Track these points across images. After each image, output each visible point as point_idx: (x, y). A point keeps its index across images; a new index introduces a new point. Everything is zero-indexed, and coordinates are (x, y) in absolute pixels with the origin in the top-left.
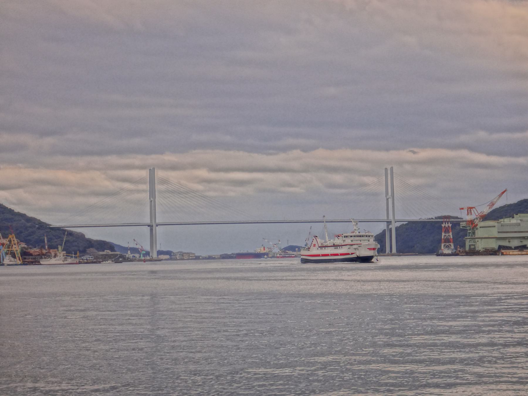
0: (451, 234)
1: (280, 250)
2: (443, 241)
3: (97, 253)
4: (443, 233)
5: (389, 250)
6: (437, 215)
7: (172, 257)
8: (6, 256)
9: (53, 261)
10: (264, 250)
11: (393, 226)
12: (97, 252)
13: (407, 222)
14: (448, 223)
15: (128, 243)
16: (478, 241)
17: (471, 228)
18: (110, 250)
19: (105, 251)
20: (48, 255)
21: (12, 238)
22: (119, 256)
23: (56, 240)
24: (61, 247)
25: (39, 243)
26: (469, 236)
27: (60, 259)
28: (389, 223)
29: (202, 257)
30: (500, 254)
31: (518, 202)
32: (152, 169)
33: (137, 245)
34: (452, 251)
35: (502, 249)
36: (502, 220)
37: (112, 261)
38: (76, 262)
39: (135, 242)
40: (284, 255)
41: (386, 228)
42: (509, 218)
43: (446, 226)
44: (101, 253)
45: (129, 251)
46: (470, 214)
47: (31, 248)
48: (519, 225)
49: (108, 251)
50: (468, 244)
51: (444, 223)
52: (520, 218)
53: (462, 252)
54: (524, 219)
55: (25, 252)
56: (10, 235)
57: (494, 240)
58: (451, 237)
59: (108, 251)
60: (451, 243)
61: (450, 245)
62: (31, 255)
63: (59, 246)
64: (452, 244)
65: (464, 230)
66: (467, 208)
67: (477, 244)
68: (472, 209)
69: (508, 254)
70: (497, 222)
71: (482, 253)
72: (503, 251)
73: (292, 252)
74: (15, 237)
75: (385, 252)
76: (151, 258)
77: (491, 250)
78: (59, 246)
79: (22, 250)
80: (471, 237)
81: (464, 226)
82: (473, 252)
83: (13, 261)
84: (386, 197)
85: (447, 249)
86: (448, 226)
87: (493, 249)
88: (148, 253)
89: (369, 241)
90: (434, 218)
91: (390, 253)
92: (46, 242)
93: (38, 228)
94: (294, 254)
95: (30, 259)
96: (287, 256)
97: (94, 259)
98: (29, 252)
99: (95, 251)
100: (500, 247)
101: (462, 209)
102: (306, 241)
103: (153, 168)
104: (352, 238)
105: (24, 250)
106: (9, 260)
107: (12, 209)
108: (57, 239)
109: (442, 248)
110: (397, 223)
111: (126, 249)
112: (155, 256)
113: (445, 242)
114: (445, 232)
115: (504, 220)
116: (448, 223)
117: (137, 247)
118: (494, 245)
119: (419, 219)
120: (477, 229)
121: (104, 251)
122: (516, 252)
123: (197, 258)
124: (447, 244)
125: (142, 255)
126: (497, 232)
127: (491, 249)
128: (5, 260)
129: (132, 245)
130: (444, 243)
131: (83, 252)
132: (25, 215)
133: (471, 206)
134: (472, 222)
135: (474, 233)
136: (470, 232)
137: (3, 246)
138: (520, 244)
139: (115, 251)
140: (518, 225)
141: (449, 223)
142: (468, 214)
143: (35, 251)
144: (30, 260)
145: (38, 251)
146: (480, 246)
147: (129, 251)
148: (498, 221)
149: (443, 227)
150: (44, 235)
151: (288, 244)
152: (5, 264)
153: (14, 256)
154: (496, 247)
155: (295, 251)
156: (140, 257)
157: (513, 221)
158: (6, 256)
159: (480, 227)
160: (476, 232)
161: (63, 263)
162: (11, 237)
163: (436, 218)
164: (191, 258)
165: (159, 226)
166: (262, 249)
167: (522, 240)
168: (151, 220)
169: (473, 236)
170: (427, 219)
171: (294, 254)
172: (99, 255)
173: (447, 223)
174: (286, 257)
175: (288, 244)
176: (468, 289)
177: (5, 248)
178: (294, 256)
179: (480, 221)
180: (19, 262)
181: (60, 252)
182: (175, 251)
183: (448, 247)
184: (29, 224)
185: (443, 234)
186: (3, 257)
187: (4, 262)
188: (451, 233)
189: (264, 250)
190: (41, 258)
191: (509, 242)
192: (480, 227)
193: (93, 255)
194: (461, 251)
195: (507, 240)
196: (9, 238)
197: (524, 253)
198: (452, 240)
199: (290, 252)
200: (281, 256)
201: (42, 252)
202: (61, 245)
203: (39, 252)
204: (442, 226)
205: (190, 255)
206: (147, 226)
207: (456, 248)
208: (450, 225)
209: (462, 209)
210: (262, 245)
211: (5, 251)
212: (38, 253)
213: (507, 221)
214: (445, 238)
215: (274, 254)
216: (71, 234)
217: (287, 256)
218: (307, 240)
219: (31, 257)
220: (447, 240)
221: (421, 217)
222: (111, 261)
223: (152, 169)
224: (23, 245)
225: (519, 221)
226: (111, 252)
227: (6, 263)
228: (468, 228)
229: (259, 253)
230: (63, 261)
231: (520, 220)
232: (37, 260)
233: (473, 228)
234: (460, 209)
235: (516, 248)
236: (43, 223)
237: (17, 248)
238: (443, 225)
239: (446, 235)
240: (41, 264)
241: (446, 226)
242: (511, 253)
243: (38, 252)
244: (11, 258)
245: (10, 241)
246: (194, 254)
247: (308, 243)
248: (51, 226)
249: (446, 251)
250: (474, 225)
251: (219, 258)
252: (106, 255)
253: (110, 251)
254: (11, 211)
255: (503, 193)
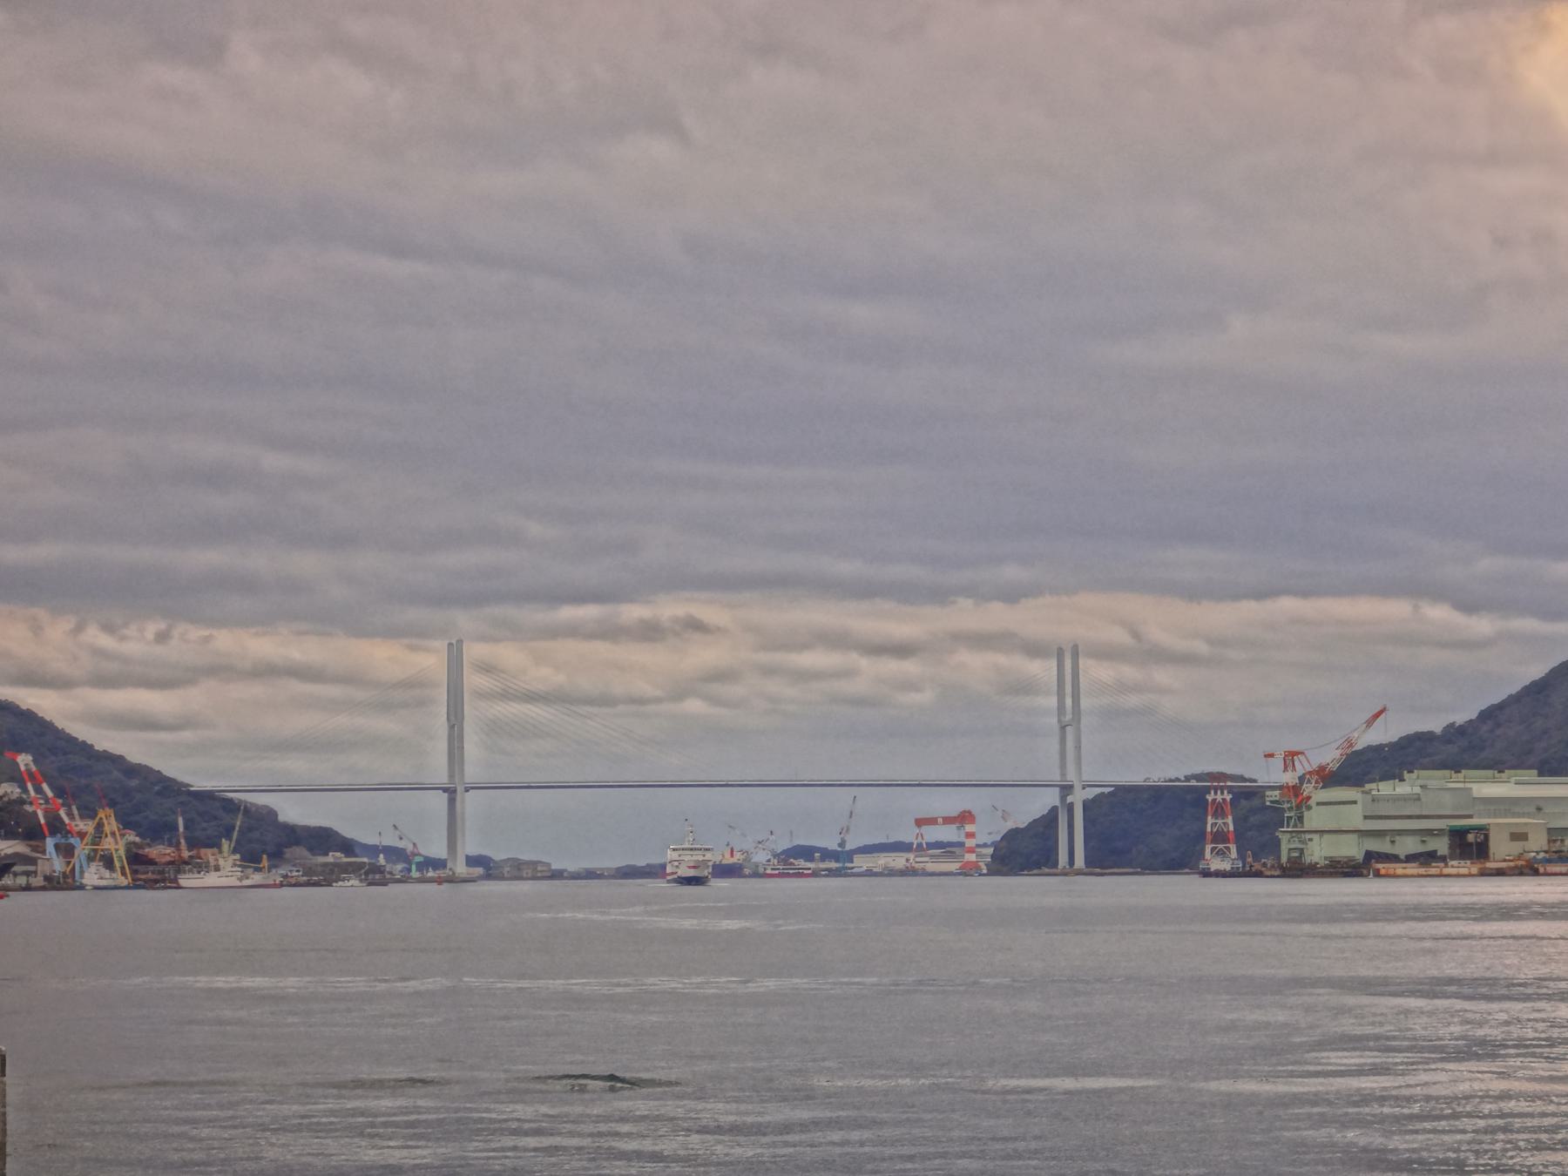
0: (1230, 820)
1: (774, 858)
2: (1209, 837)
3: (310, 859)
4: (1209, 818)
5: (1067, 860)
6: (1198, 770)
7: (490, 872)
8: (89, 864)
9: (212, 879)
10: (732, 855)
11: (1078, 798)
12: (311, 857)
13: (1113, 789)
14: (1222, 793)
15: (380, 833)
16: (1311, 840)
17: (1294, 804)
18: (342, 853)
19: (331, 854)
20: (198, 863)
21: (107, 818)
22: (367, 867)
23: (205, 825)
24: (228, 842)
25: (160, 831)
26: (1288, 827)
27: (230, 874)
28: (1066, 789)
29: (570, 872)
30: (1371, 876)
31: (1401, 738)
32: (454, 642)
33: (401, 839)
34: (1233, 864)
35: (1373, 861)
36: (1373, 786)
37: (361, 881)
38: (273, 882)
39: (397, 832)
40: (783, 869)
41: (1057, 803)
42: (1392, 781)
43: (1216, 799)
44: (321, 859)
45: (382, 856)
46: (1290, 769)
47: (149, 846)
48: (1418, 798)
49: (338, 854)
50: (1287, 845)
51: (1212, 792)
52: (1420, 782)
53: (1273, 867)
54: (1433, 784)
55: (137, 854)
56: (101, 810)
57: (1355, 836)
58: (1231, 828)
59: (339, 854)
60: (1229, 843)
61: (1228, 848)
62: (151, 862)
63: (223, 840)
64: (1233, 848)
65: (1276, 810)
66: (1283, 753)
67: (1308, 846)
68: (1295, 757)
69: (1392, 873)
70: (1363, 792)
71: (1324, 870)
72: (1379, 866)
73: (805, 861)
74: (113, 816)
75: (1055, 865)
76: (451, 873)
77: (1346, 863)
78: (223, 840)
79: (128, 851)
80: (1293, 827)
81: (1277, 801)
82: (1298, 869)
83: (108, 878)
84: (1059, 721)
85: (1219, 859)
86: (1224, 800)
87: (1351, 859)
88: (438, 864)
89: (704, 856)
90: (1183, 779)
91: (1068, 867)
92: (181, 829)
93: (159, 793)
94: (810, 869)
95: (150, 874)
96: (791, 871)
97: (302, 876)
98: (146, 856)
99: (306, 853)
100: (1370, 856)
101: (1271, 756)
102: (840, 833)
103: (458, 641)
104: (681, 852)
105: (135, 850)
106: (96, 876)
107: (89, 742)
108: (205, 822)
109: (1208, 855)
110: (1087, 789)
111: (374, 850)
112: (461, 869)
113: (1214, 841)
114: (1215, 815)
115: (1378, 785)
116: (1222, 793)
117: (400, 844)
118: (1351, 849)
119: (1145, 781)
120: (1309, 808)
121: (328, 855)
122: (1412, 869)
123: (557, 875)
124: (1221, 846)
125: (414, 867)
126: (1362, 818)
127: (1345, 860)
128: (86, 875)
129: (390, 840)
130: (1212, 843)
131: (277, 856)
132: (121, 758)
133: (1296, 749)
134: (1295, 790)
135: (1301, 819)
136: (1291, 817)
137: (82, 839)
138: (1421, 849)
139: (356, 856)
140: (1415, 800)
141: (1226, 792)
142: (1286, 769)
143: (159, 852)
144: (150, 876)
145: (168, 851)
146: (1318, 852)
147: (382, 856)
148: (1363, 789)
149: (1210, 800)
150: (174, 813)
151: (791, 841)
152: (87, 885)
153: (108, 862)
154: (1360, 857)
155: (812, 860)
156: (409, 870)
157: (1402, 789)
158: (89, 864)
159: (1318, 804)
160: (1306, 814)
161: (238, 884)
162: (103, 816)
163: (1187, 779)
164: (539, 875)
165: (471, 791)
166: (727, 855)
167: (1424, 839)
168: (451, 776)
169: (1299, 825)
170: (1166, 782)
171: (810, 869)
172: (317, 865)
173: (1219, 792)
174: (789, 875)
175: (791, 841)
176: (951, 988)
177: (87, 844)
178: (810, 872)
179: (1316, 788)
180: (124, 881)
181: (226, 854)
182: (498, 856)
183: (1222, 854)
184: (134, 783)
185: (1210, 820)
186: (81, 867)
187: (84, 881)
188: (1230, 818)
189: (732, 855)
190: (178, 871)
191: (1393, 842)
192: (1318, 804)
193: (300, 865)
194: (1269, 865)
195: (1388, 838)
196: (98, 818)
197: (1433, 871)
198: (1231, 837)
199: (802, 863)
200: (777, 872)
201: (180, 856)
202: (229, 838)
203: (172, 854)
204: (1207, 800)
205: (539, 868)
206: (441, 791)
207: (1242, 856)
208: (1228, 797)
209: (1271, 756)
210: (728, 845)
211: (87, 852)
212: (168, 859)
213: (1385, 788)
214: (1215, 830)
215: (757, 866)
216: (248, 811)
217: (791, 871)
218: (844, 831)
219: (151, 868)
220: (1220, 837)
221: (1148, 776)
222: (357, 882)
223: (454, 642)
224: (132, 837)
225: (1417, 790)
226: (346, 857)
227: (89, 883)
228: (1286, 806)
229: (717, 863)
230: (240, 879)
231: (1421, 786)
232: (167, 875)
233: (1299, 807)
234: (1265, 756)
235: (1411, 858)
236: (169, 779)
237: (116, 846)
238: (1210, 798)
239: (1216, 824)
240: (179, 887)
241: (1216, 799)
242: (1400, 871)
243: (169, 854)
244: (103, 870)
245: (99, 827)
246: (549, 865)
247: (846, 838)
248: (192, 789)
249: (1217, 864)
250: (1300, 798)
251: (613, 877)
252: (335, 865)
253: (343, 855)
254: (85, 748)
255: (1378, 717)
